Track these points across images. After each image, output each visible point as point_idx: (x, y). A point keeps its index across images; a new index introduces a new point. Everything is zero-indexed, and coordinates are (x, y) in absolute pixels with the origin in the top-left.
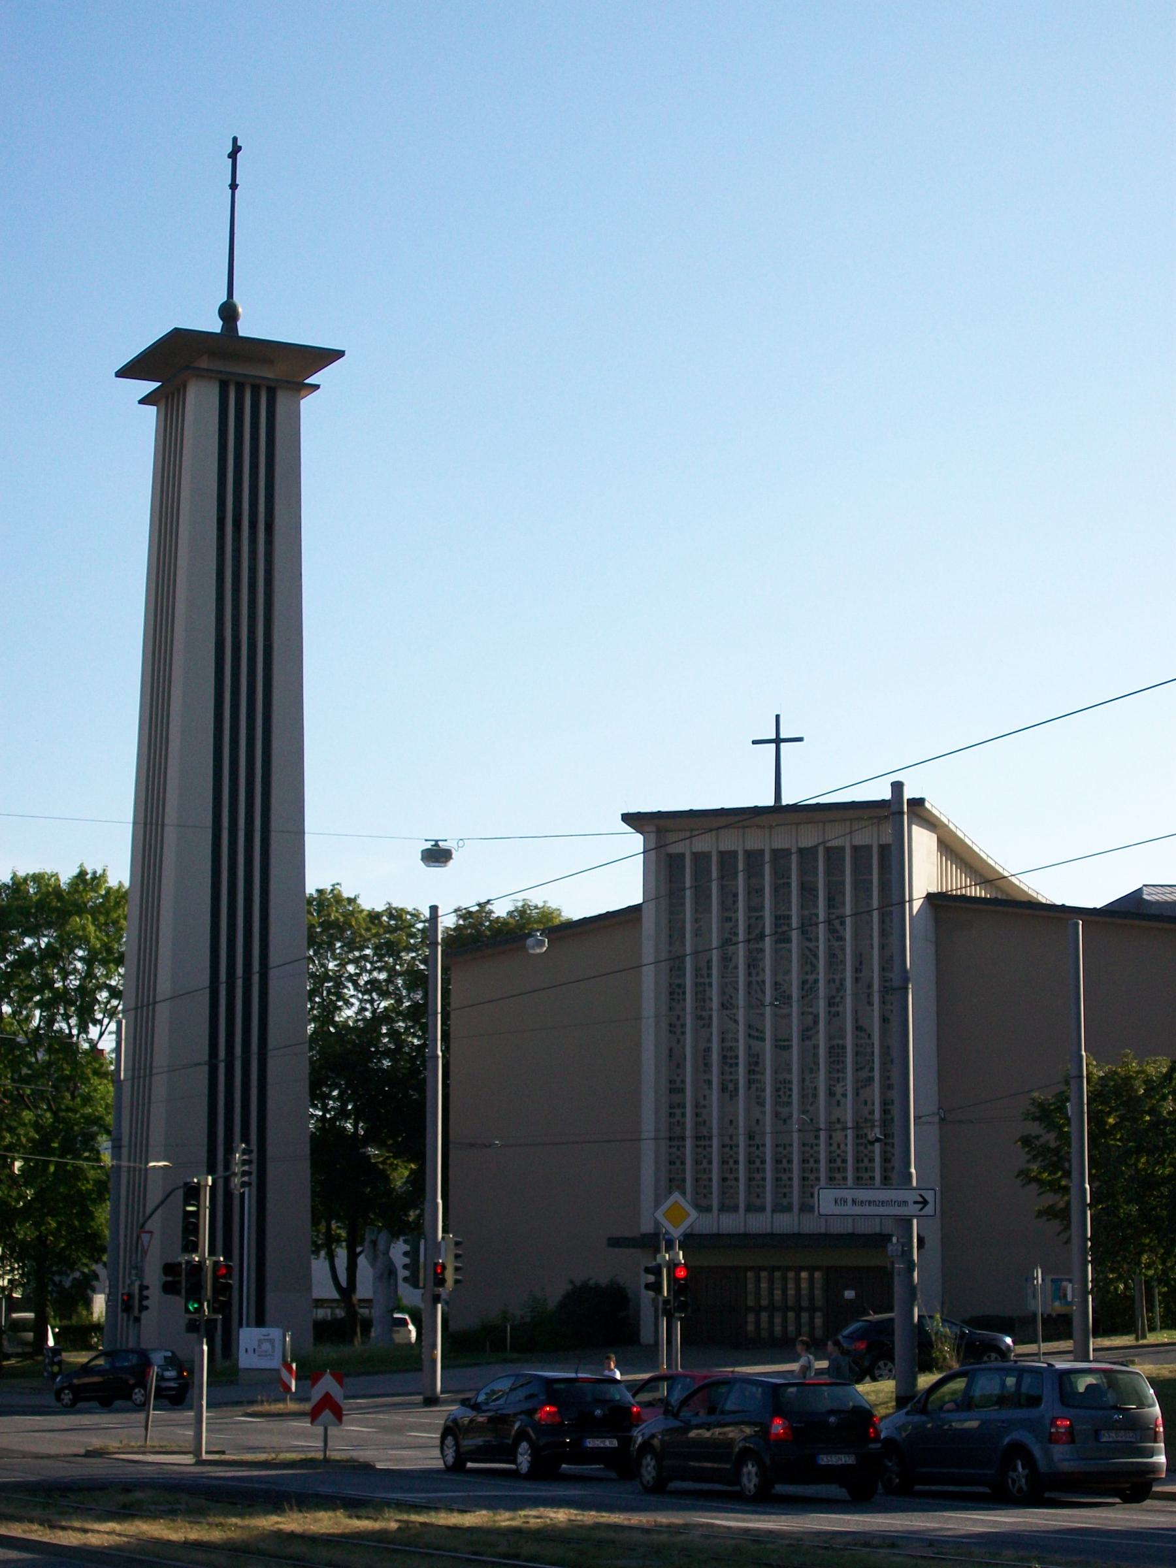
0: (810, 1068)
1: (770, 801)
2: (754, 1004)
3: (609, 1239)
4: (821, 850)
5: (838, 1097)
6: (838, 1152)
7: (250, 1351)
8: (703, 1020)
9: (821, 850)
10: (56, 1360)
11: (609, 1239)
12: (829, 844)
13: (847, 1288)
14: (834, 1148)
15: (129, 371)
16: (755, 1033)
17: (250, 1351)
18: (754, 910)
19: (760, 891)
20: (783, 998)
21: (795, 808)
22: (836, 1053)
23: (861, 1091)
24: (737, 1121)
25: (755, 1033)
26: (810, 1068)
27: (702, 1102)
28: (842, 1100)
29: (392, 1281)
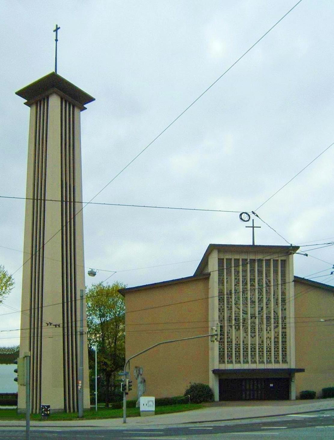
0: (261, 323)
1: (252, 244)
2: (245, 304)
3: (304, 371)
4: (272, 260)
5: (268, 331)
6: (268, 346)
7: (145, 405)
8: (230, 309)
9: (272, 260)
10: (48, 409)
11: (304, 371)
12: (274, 259)
13: (271, 383)
14: (267, 345)
15: (20, 93)
16: (245, 312)
17: (145, 405)
18: (244, 277)
19: (238, 272)
20: (253, 302)
21: (257, 246)
22: (268, 318)
23: (275, 329)
24: (259, 338)
25: (245, 312)
26: (261, 323)
27: (229, 332)
28: (269, 332)
29: (145, 383)
